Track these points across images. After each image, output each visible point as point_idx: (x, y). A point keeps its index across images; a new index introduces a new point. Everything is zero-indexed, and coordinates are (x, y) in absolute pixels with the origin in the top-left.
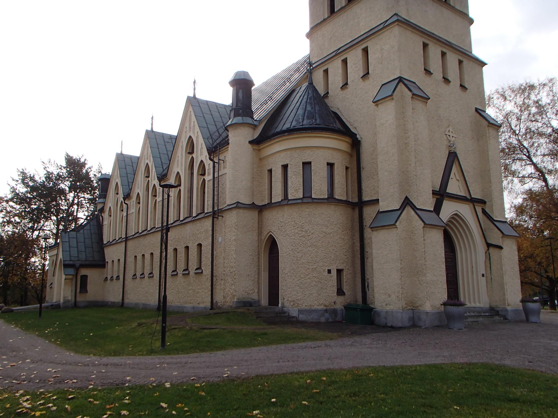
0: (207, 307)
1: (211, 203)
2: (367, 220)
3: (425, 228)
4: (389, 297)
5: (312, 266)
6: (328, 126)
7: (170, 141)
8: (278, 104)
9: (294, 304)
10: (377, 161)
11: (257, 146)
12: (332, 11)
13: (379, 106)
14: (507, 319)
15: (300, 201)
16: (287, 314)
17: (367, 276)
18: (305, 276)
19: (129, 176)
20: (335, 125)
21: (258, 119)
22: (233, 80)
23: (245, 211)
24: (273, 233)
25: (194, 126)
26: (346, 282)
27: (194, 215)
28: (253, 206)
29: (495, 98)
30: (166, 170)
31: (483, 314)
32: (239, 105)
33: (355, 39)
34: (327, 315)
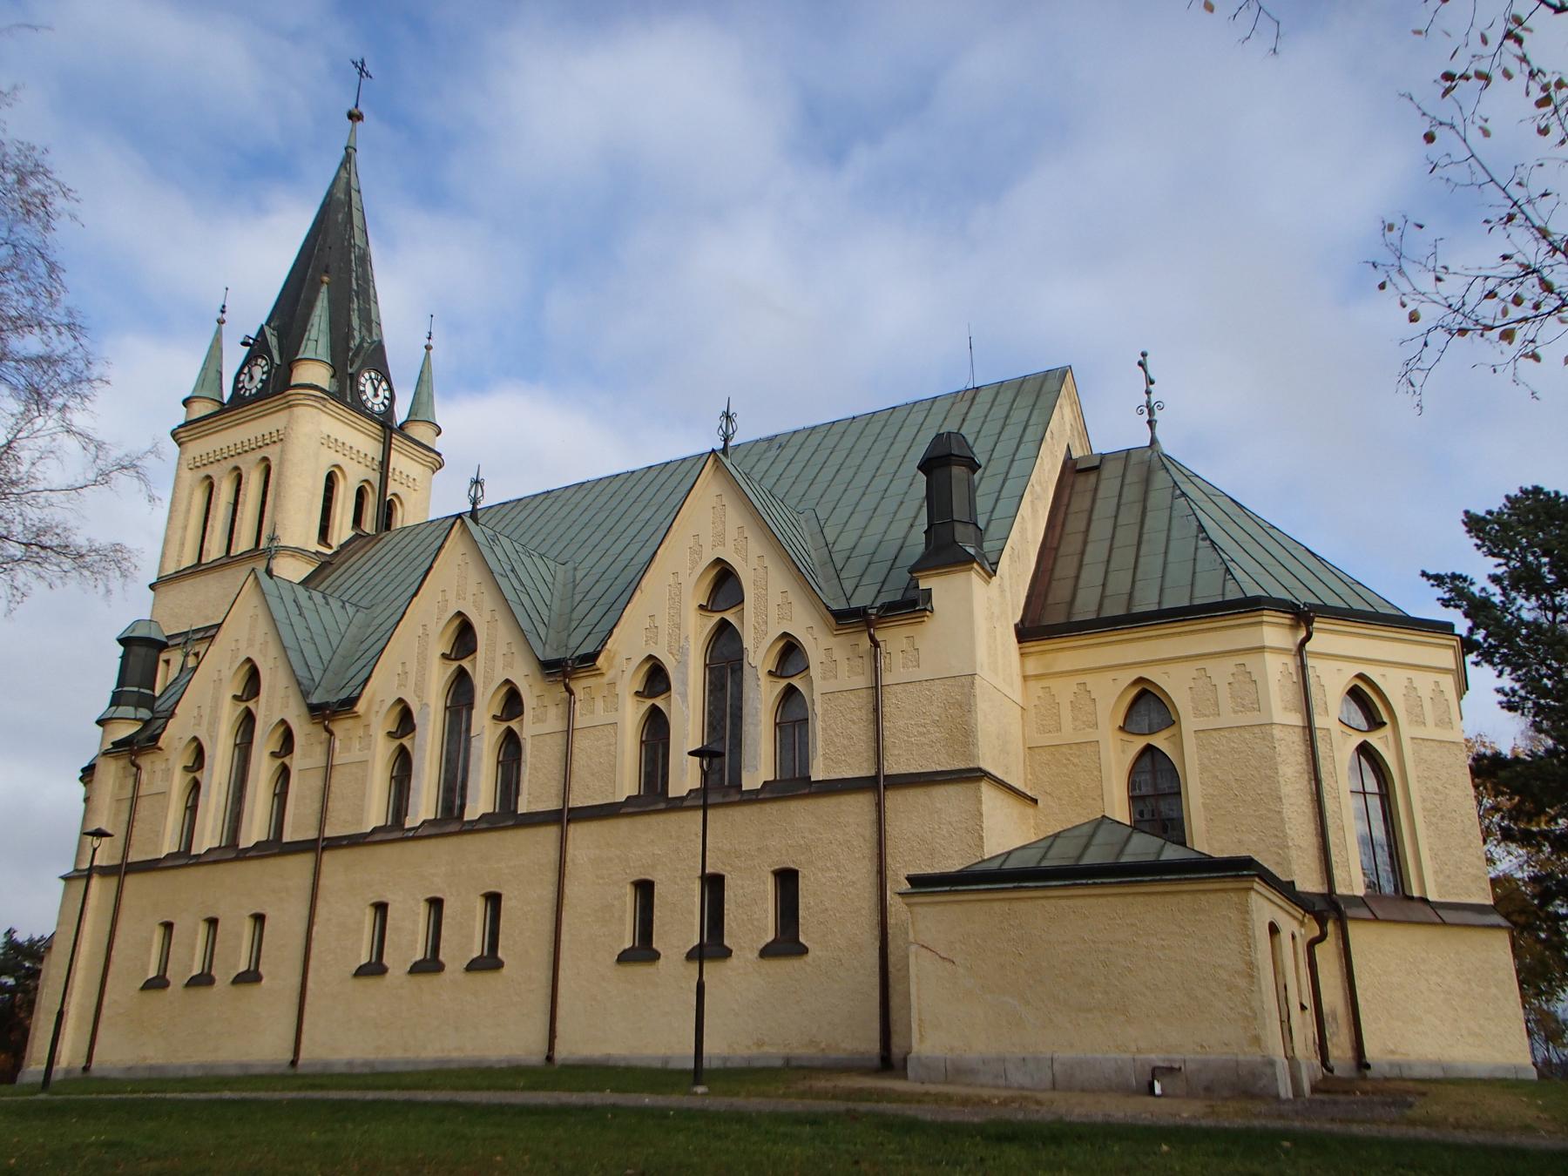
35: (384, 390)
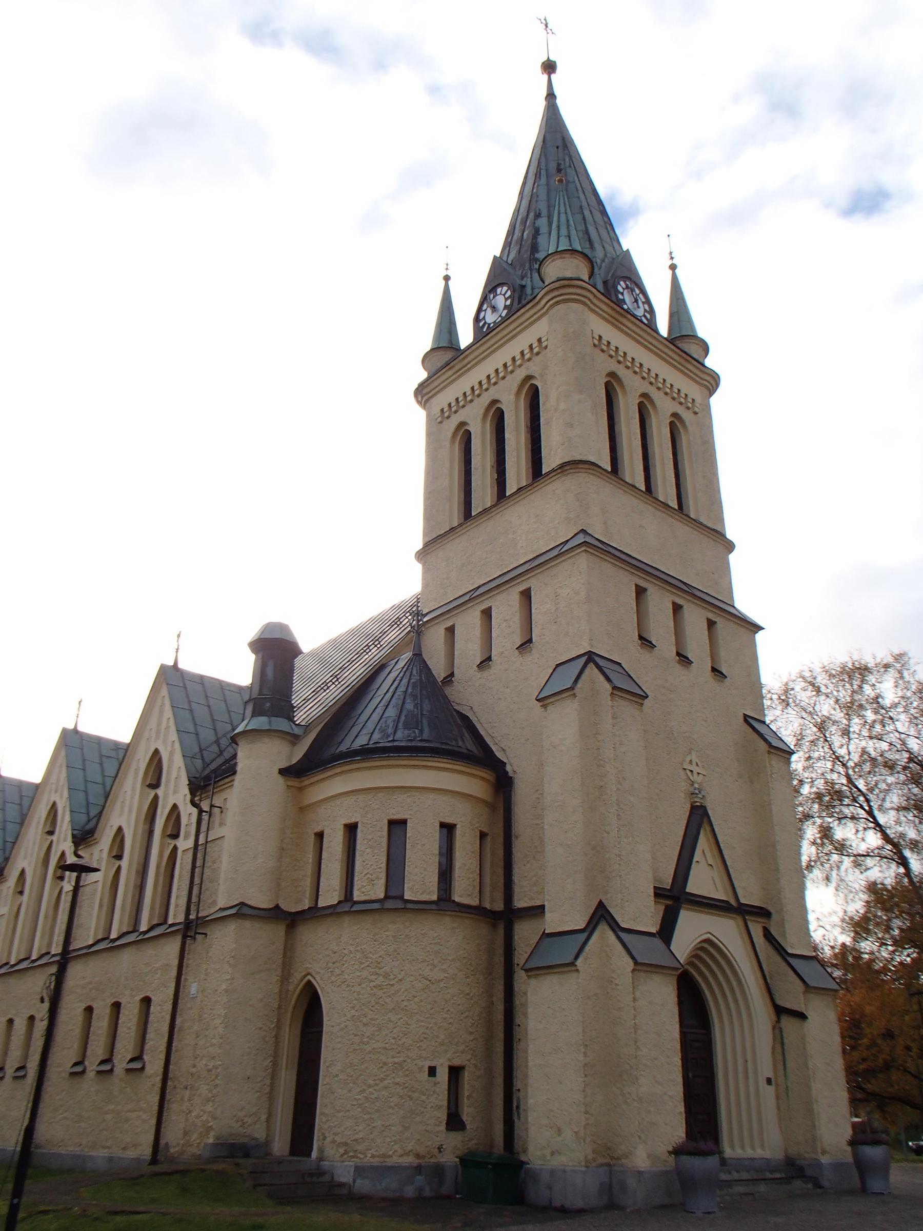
0: (142, 1157)
1: (183, 901)
2: (521, 952)
3: (636, 973)
4: (559, 1135)
5: (393, 1057)
6: (446, 744)
7: (113, 754)
8: (349, 693)
9: (346, 1152)
10: (543, 823)
11: (296, 780)
12: (467, 514)
13: (548, 708)
14: (820, 1187)
15: (376, 906)
16: (326, 1178)
17: (517, 1084)
18: (378, 1082)
19: (10, 826)
20: (460, 743)
21: (303, 724)
22: (256, 640)
23: (257, 925)
24: (314, 978)
25: (167, 727)
26: (468, 1097)
27: (143, 927)
28: (275, 914)
29: (797, 688)
30: (95, 821)
31: (768, 1175)
32: (265, 691)
33: (508, 572)
34: (420, 1180)
35: (643, 302)
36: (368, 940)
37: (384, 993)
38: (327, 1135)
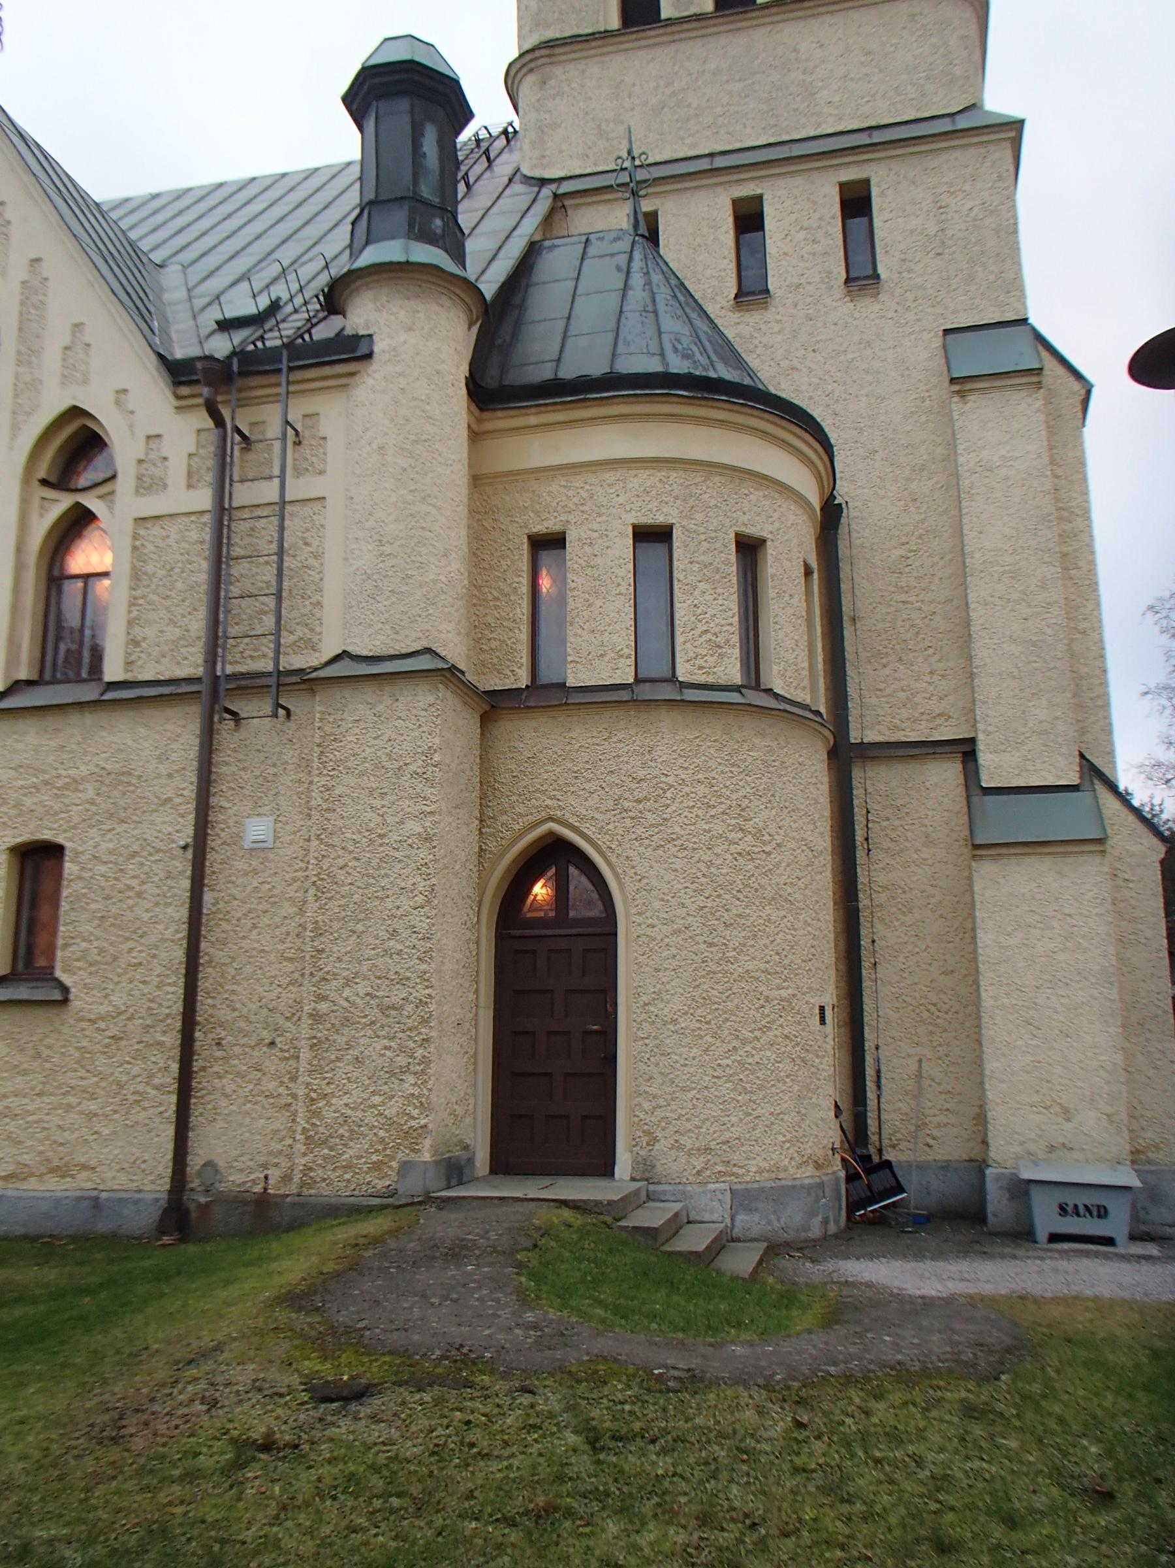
15: (624, 695)
18: (758, 1034)
24: (576, 830)
36: (720, 764)
37: (757, 867)
38: (658, 1134)
